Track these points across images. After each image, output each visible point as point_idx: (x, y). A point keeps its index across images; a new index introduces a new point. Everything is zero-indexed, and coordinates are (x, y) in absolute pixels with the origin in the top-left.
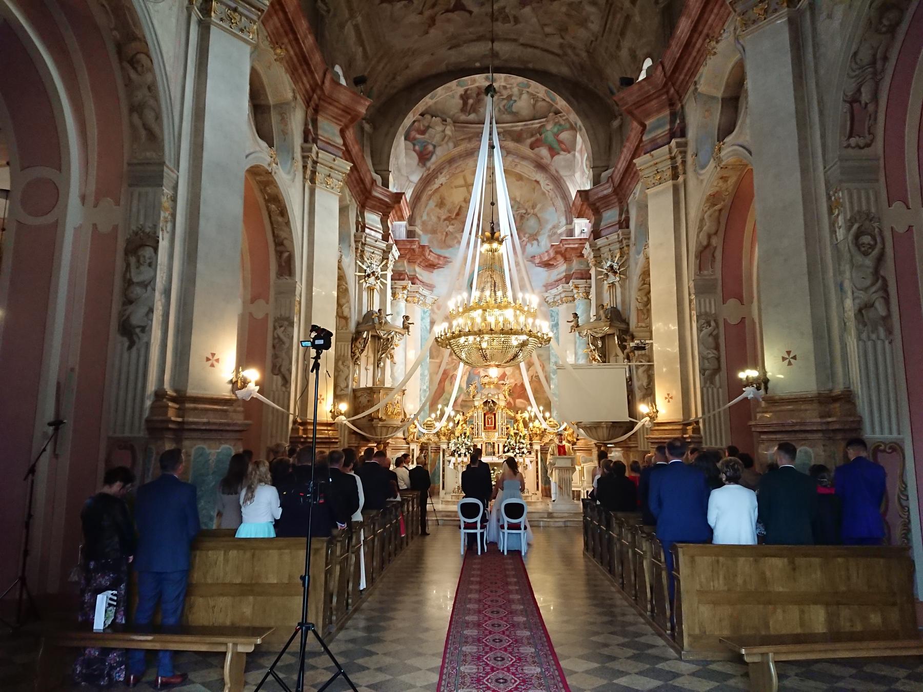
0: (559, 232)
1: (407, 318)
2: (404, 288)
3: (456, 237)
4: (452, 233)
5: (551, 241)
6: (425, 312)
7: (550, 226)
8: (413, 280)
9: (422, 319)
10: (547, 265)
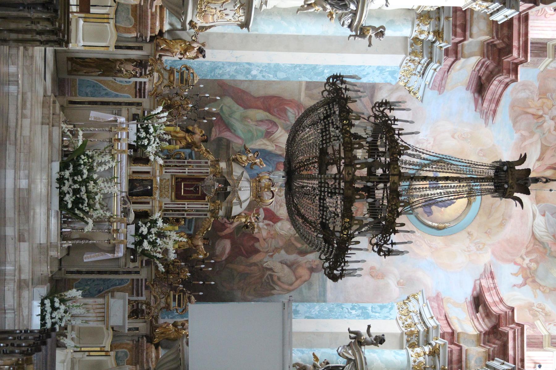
0: (538, 323)
1: (380, 33)
2: (438, 34)
3: (532, 133)
4: (540, 126)
5: (521, 308)
6: (392, 73)
7: (549, 306)
8: (455, 52)
9: (381, 70)
10: (478, 301)
